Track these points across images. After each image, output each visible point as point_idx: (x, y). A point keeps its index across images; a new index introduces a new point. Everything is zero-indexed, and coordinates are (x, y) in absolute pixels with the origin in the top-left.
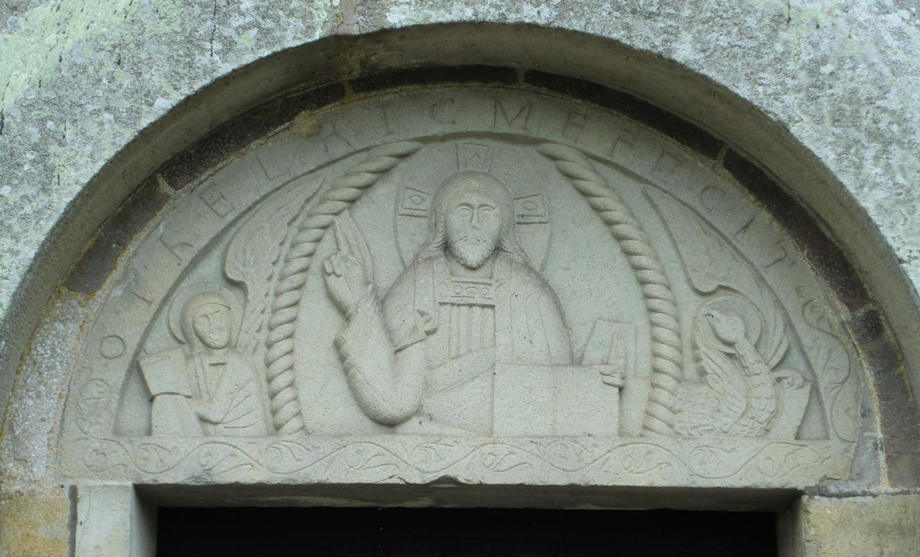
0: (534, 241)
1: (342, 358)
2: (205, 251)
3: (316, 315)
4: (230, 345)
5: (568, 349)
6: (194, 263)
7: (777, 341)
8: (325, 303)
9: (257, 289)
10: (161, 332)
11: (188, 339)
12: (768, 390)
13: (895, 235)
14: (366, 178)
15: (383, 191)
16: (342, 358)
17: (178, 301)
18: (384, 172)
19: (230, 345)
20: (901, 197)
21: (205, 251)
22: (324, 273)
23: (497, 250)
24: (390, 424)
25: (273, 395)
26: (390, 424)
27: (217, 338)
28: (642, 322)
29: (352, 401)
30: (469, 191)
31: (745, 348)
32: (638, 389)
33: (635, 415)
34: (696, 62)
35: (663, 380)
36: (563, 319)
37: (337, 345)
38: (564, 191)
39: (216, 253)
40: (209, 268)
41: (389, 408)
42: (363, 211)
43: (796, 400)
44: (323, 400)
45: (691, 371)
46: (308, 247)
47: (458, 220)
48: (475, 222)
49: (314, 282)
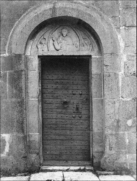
0: (70, 34)
2: (42, 36)
3: (51, 41)
8: (52, 40)
9: (47, 39)
11: (41, 43)
13: (102, 41)
18: (57, 29)
20: (68, 118)
22: (52, 37)
23: (67, 35)
24: (58, 50)
25: (48, 48)
26: (58, 50)
27: (43, 43)
31: (87, 44)
33: (78, 49)
35: (81, 46)
36: (54, 47)
37: (53, 44)
39: (43, 36)
43: (91, 48)
44: (52, 48)
48: (65, 32)
49: (51, 38)
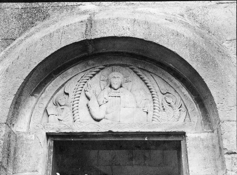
1: (88, 108)
3: (83, 100)
12: (178, 112)
17: (55, 97)
24: (98, 120)
26: (98, 120)
30: (115, 74)
31: (172, 104)
32: (151, 113)
37: (87, 105)
40: (61, 91)
41: (98, 117)
42: (93, 79)
44: (83, 114)
45: (162, 109)
49: (83, 92)
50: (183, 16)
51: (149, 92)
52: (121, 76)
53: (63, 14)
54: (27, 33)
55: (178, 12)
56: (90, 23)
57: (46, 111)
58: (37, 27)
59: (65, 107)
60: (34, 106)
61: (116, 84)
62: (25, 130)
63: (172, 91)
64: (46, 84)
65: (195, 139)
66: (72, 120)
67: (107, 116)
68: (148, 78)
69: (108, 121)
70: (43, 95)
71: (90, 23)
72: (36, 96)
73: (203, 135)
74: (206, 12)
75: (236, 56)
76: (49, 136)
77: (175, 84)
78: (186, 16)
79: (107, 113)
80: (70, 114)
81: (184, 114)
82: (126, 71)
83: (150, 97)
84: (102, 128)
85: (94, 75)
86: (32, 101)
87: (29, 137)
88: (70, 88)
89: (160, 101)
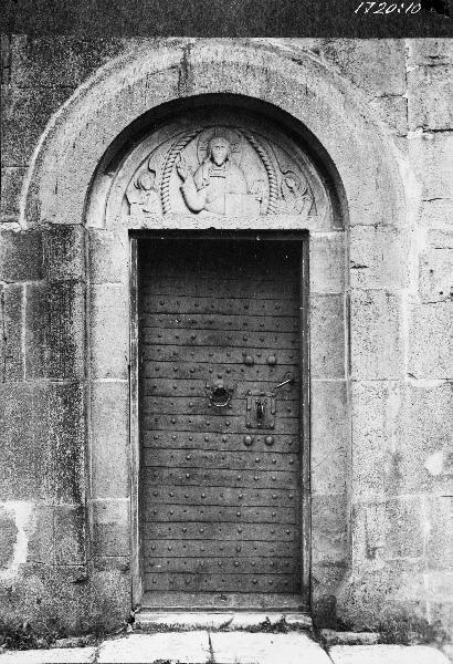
0: (237, 157)
1: (183, 193)
2: (143, 162)
3: (174, 181)
4: (152, 188)
5: (284, 534)
6: (141, 165)
7: (304, 186)
10: (132, 184)
12: (301, 202)
14: (188, 139)
15: (193, 143)
16: (183, 193)
17: (137, 176)
19: (152, 188)
21: (143, 162)
23: (227, 160)
24: (196, 212)
26: (196, 212)
27: (147, 187)
28: (267, 181)
29: (91, 208)
30: (219, 142)
31: (295, 189)
32: (265, 201)
34: (114, 542)
37: (181, 189)
38: (248, 148)
40: (144, 166)
41: (195, 208)
42: (188, 147)
44: (175, 202)
45: (280, 195)
46: (172, 160)
47: (215, 151)
48: (221, 150)
49: (174, 169)
50: (318, 52)
51: (264, 170)
52: (226, 144)
53: (144, 46)
54: (92, 79)
55: (311, 46)
56: (184, 68)
57: (125, 196)
58: (106, 66)
59: (151, 192)
60: (111, 189)
61: (220, 156)
62: (100, 226)
63: (296, 170)
64: (122, 158)
65: (320, 240)
66: (160, 212)
67: (207, 206)
68: (264, 149)
69: (212, 214)
70: (121, 174)
71: (184, 68)
72: (111, 176)
73: (330, 235)
74: (351, 46)
75: (313, 456)
76: (131, 232)
77: (301, 160)
78: (322, 53)
79: (207, 201)
80: (159, 202)
81: (309, 204)
82: (232, 135)
83: (265, 176)
84: (202, 223)
85: (189, 142)
86: (106, 182)
87: (107, 234)
88: (158, 162)
89: (279, 183)
